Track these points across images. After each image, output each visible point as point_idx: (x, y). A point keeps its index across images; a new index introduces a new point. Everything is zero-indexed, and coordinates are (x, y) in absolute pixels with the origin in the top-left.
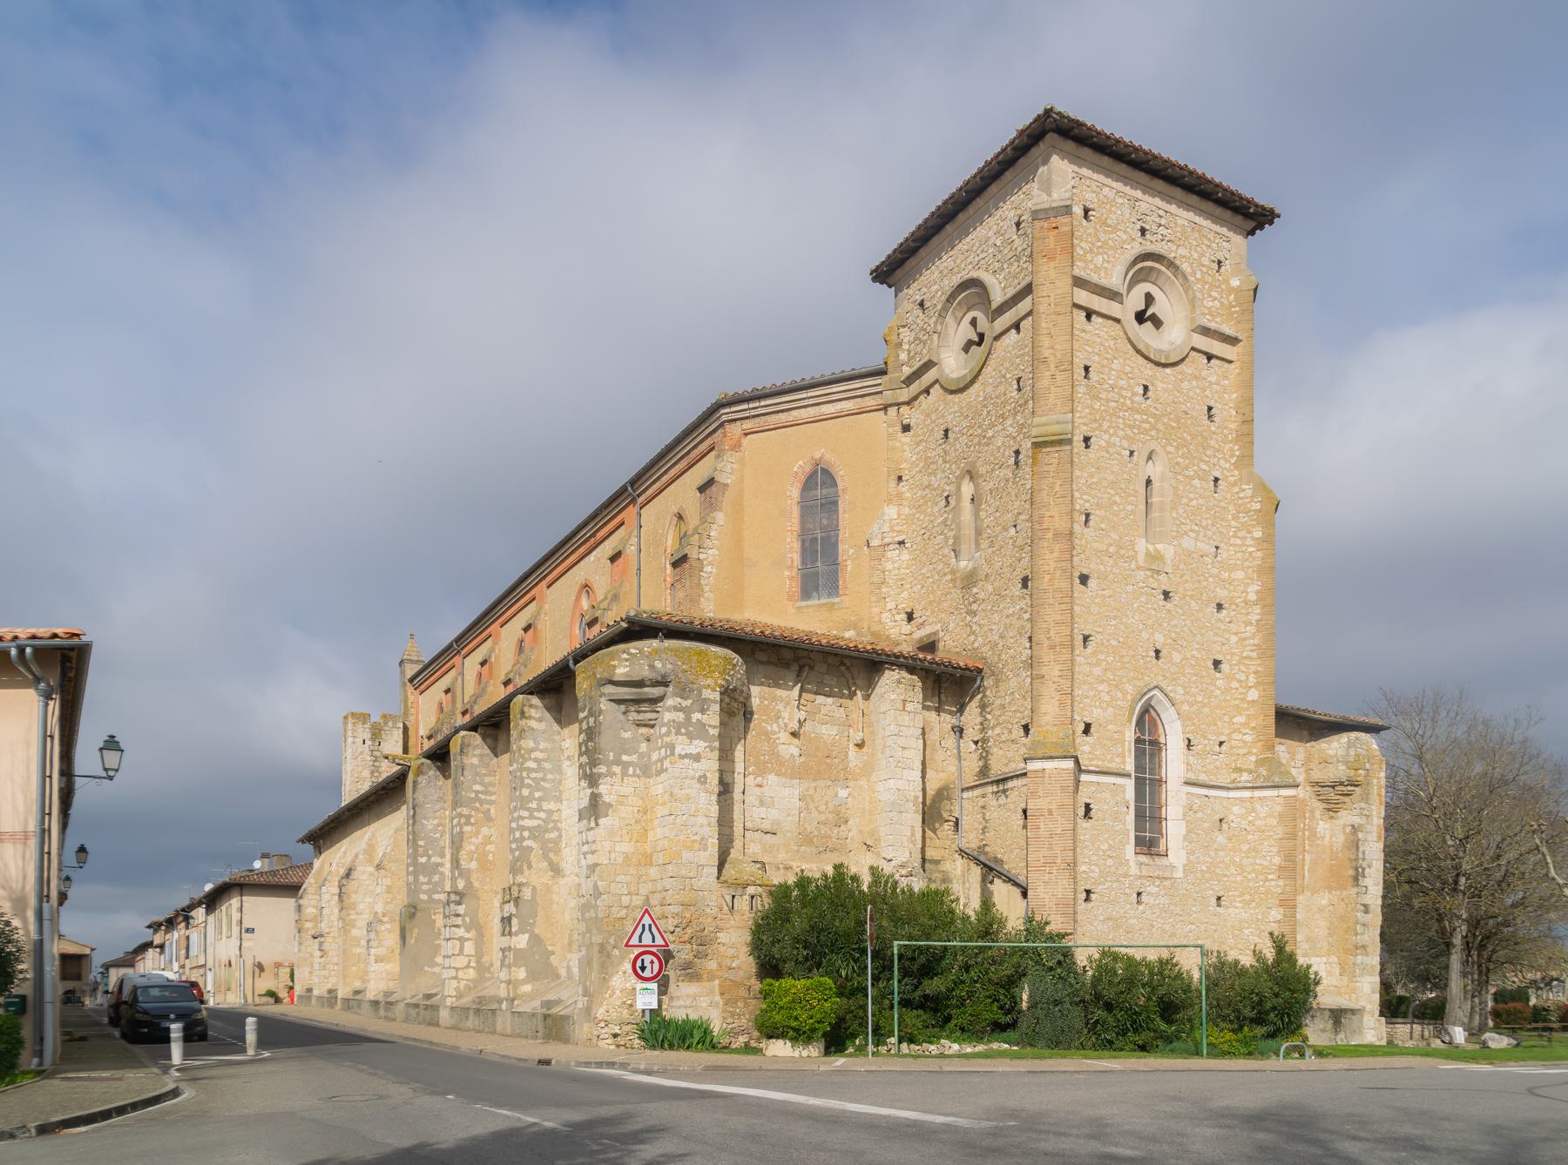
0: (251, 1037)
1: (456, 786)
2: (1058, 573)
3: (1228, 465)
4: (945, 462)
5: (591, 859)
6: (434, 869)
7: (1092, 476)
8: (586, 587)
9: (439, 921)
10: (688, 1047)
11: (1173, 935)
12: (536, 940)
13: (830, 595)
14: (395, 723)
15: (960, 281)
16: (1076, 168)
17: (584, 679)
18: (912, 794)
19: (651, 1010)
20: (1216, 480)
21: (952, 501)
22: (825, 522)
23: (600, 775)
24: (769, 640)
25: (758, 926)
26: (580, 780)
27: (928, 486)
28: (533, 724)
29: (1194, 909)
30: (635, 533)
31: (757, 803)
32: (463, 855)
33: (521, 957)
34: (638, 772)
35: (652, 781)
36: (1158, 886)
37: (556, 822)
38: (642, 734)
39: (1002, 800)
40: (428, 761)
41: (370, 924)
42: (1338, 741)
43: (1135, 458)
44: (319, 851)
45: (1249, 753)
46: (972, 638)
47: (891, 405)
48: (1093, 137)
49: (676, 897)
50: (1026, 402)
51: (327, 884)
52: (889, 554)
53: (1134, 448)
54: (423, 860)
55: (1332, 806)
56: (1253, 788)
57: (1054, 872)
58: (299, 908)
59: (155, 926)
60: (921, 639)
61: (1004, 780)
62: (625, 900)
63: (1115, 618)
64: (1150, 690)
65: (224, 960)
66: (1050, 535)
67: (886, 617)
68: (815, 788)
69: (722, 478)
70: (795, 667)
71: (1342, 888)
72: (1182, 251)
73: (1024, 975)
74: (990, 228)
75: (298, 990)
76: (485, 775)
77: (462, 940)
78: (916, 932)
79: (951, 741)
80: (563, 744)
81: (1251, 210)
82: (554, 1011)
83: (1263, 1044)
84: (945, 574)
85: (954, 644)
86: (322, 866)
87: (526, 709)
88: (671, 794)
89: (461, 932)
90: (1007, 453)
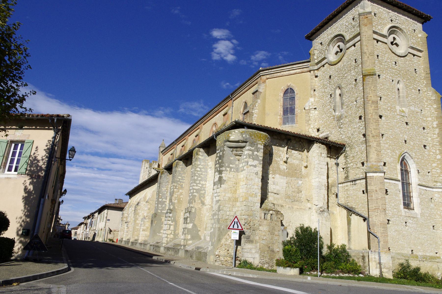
1: (173, 177)
2: (374, 113)
3: (422, 86)
5: (218, 198)
7: (381, 86)
8: (215, 124)
9: (163, 219)
12: (195, 226)
14: (156, 163)
16: (372, 4)
18: (324, 183)
20: (419, 90)
21: (333, 96)
22: (291, 103)
26: (215, 172)
27: (324, 92)
29: (425, 229)
30: (231, 108)
31: (272, 183)
32: (173, 198)
34: (235, 170)
35: (239, 174)
38: (237, 158)
40: (165, 170)
41: (142, 219)
43: (394, 82)
44: (130, 197)
46: (341, 136)
49: (246, 213)
50: (358, 65)
51: (131, 207)
52: (311, 112)
54: (160, 200)
57: (379, 212)
59: (85, 218)
61: (355, 181)
62: (228, 213)
63: (391, 129)
64: (404, 153)
65: (100, 228)
66: (370, 102)
67: (310, 130)
68: (291, 180)
69: (260, 90)
70: (286, 141)
72: (403, 26)
74: (344, 21)
77: (170, 225)
79: (335, 167)
80: (209, 163)
81: (424, 16)
84: (331, 117)
86: (131, 202)
87: (198, 152)
89: (170, 222)
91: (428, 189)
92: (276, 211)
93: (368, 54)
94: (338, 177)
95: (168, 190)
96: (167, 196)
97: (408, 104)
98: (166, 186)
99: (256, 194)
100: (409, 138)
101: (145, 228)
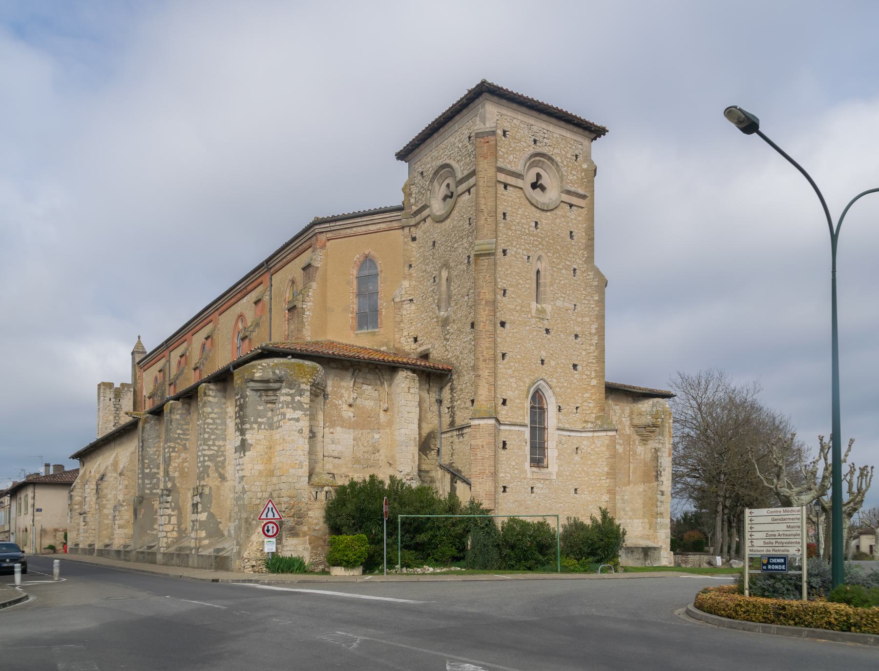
0: (56, 571)
3: (581, 262)
4: (433, 259)
5: (241, 473)
6: (153, 476)
7: (507, 270)
8: (241, 317)
9: (156, 505)
10: (291, 572)
11: (551, 509)
12: (211, 516)
13: (373, 327)
15: (441, 164)
17: (239, 378)
19: (272, 553)
20: (575, 270)
21: (437, 280)
23: (246, 429)
24: (337, 357)
25: (329, 508)
26: (235, 432)
27: (425, 271)
28: (210, 399)
30: (269, 289)
32: (171, 469)
33: (203, 525)
34: (267, 427)
35: (274, 432)
36: (543, 483)
37: (223, 452)
38: (269, 408)
39: (461, 439)
40: (151, 416)
41: (115, 507)
42: (647, 403)
45: (592, 413)
46: (447, 353)
47: (406, 226)
48: (507, 94)
50: (473, 231)
51: (89, 483)
53: (530, 254)
55: (645, 438)
56: (593, 431)
58: (71, 497)
60: (421, 352)
61: (462, 429)
62: (259, 495)
63: (519, 344)
64: (538, 381)
65: (22, 527)
66: (483, 302)
67: (403, 339)
69: (316, 264)
70: (351, 370)
71: (650, 482)
72: (556, 151)
73: (470, 531)
75: (70, 544)
76: (184, 424)
77: (170, 516)
78: (412, 510)
79: (435, 408)
82: (221, 554)
83: (593, 566)
84: (433, 318)
85: (438, 355)
86: (85, 472)
87: (207, 391)
88: (284, 439)
89: (169, 511)
90: (464, 257)
91: (572, 434)
92: (335, 486)
93: (486, 214)
94: (440, 422)
95: (159, 452)
96: (159, 463)
97: (552, 296)
98: (156, 445)
99: (300, 463)
100: (549, 355)
101: (121, 522)
